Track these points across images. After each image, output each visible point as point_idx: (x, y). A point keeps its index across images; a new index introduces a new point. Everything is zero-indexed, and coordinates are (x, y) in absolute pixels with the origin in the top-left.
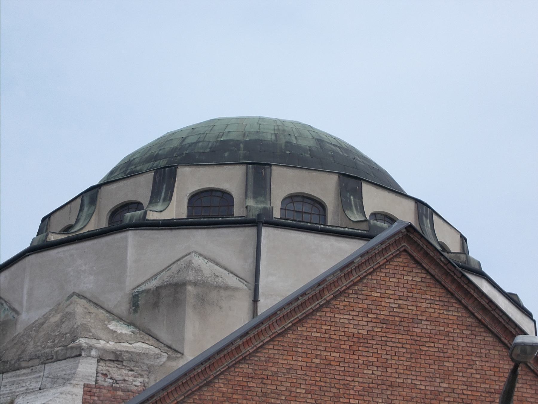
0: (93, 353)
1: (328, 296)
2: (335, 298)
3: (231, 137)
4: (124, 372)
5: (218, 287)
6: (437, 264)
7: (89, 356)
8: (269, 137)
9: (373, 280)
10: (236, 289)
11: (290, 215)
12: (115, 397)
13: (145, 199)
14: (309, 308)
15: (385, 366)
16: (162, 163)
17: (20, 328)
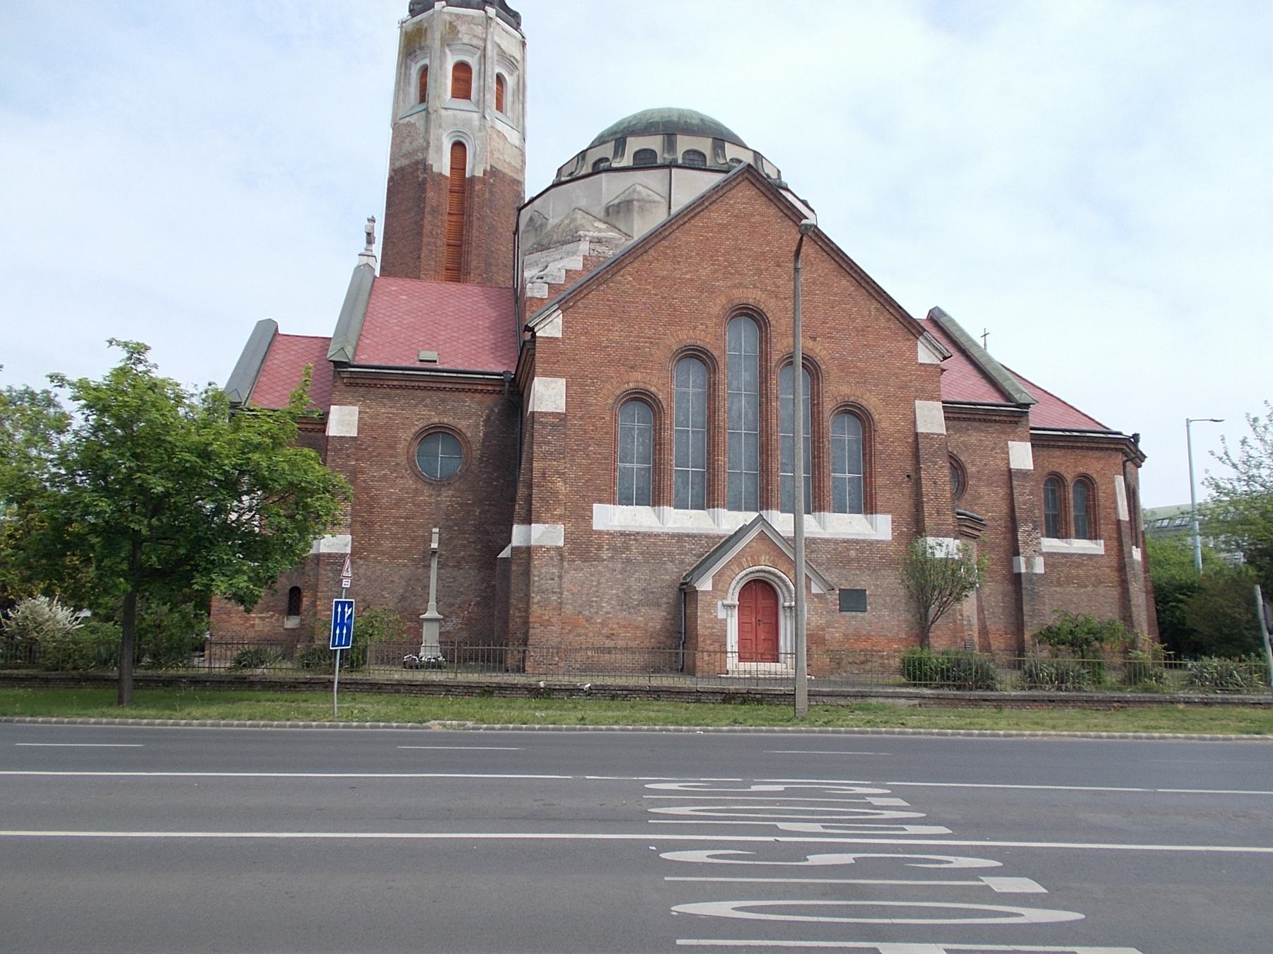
0: (587, 238)
1: (707, 204)
2: (710, 204)
4: (604, 248)
6: (764, 185)
7: (585, 240)
8: (675, 119)
10: (659, 202)
12: (599, 261)
13: (610, 155)
14: (697, 211)
16: (619, 136)
17: (549, 227)
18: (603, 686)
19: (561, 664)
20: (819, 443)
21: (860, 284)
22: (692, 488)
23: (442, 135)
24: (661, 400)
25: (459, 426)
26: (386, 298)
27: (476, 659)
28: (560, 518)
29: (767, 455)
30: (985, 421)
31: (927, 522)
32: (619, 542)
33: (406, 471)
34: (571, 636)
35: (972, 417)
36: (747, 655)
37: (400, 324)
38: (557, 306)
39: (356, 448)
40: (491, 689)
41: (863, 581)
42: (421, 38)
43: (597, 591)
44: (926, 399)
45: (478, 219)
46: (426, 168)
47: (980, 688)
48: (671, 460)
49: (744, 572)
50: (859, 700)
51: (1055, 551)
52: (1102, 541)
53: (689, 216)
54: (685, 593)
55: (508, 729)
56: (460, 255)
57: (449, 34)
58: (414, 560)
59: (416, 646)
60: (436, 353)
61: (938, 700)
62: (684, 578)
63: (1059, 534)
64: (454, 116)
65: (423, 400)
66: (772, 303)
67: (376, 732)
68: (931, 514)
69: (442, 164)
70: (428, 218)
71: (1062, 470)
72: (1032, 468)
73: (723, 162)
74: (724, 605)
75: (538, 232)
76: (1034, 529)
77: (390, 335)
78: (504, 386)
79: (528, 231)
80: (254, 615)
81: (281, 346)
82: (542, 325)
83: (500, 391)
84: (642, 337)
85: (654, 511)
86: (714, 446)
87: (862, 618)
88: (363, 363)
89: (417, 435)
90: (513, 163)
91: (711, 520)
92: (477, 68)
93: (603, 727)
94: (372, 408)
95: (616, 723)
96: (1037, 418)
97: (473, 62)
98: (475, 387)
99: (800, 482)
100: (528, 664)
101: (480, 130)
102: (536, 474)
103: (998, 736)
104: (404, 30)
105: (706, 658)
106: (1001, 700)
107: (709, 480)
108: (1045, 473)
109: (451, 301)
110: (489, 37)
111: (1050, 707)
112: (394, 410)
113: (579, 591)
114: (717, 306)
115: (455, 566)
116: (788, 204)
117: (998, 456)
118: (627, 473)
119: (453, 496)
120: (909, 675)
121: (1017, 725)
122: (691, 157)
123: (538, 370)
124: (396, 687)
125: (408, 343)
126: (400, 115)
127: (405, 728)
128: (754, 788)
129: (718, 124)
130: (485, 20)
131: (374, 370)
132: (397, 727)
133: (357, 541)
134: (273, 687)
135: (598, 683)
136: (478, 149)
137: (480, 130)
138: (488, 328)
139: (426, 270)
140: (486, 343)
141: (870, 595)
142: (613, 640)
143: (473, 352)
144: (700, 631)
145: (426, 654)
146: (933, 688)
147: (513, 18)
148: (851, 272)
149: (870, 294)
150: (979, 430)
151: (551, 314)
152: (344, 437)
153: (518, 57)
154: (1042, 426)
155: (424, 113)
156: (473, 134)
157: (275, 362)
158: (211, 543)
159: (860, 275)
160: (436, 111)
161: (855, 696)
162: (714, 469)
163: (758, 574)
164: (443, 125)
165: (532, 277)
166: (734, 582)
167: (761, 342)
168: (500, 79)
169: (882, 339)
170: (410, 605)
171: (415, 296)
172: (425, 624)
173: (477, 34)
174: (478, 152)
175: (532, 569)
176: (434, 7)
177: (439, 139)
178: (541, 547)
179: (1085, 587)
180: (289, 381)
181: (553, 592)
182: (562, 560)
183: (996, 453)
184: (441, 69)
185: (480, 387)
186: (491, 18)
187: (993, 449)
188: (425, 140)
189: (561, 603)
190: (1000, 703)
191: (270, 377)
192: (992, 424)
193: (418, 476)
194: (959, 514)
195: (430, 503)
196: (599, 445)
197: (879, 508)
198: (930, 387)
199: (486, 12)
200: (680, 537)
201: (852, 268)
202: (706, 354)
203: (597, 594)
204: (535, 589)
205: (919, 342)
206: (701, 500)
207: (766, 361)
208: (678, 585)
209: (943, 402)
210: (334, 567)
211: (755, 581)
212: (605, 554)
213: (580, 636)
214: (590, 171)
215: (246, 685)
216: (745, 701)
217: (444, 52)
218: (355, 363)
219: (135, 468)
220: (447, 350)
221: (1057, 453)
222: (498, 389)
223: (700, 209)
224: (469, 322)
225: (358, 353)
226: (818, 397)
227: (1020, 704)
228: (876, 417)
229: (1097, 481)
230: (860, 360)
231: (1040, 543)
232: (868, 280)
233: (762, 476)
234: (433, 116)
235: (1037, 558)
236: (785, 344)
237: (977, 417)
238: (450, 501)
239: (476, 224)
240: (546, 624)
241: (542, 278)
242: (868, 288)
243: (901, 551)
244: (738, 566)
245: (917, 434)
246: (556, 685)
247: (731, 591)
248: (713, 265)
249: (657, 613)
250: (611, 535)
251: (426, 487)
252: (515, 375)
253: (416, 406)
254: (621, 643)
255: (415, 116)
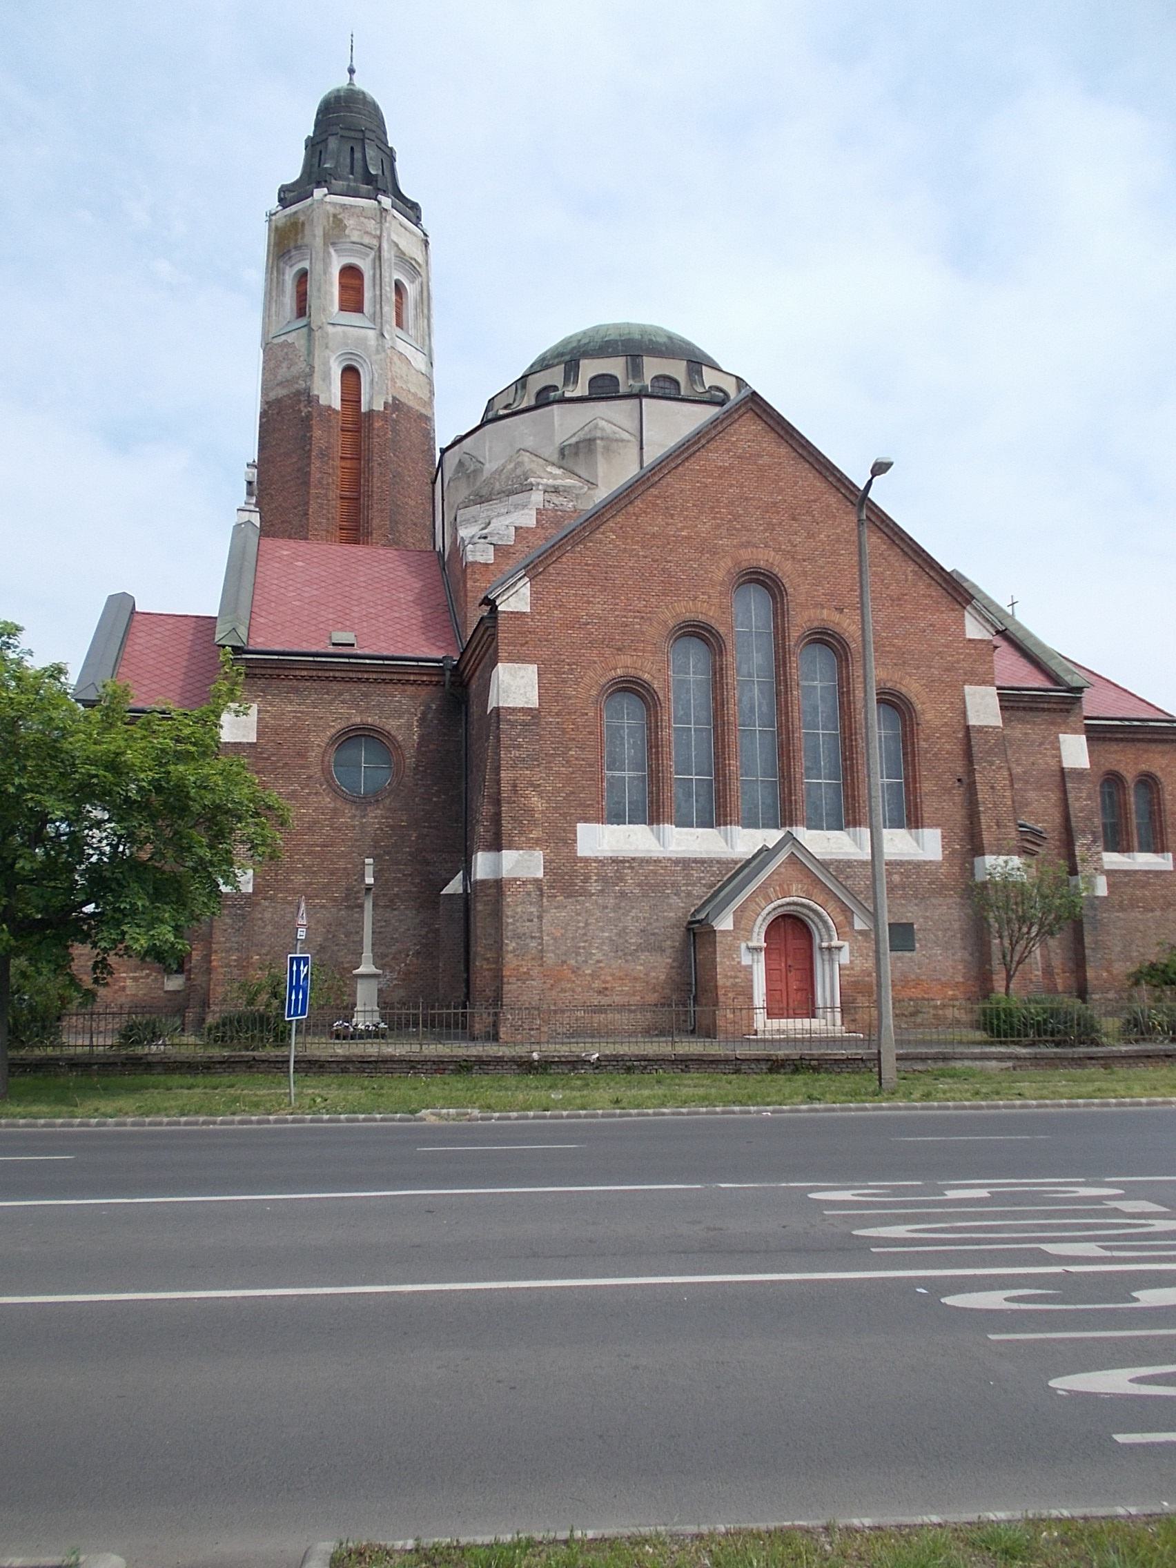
0: (540, 487)
1: (703, 441)
2: (708, 442)
3: (612, 337)
4: (561, 499)
5: (617, 440)
6: (772, 417)
7: (538, 489)
8: (637, 336)
9: (731, 430)
10: (628, 441)
11: (657, 390)
12: (556, 515)
13: (560, 384)
14: (691, 450)
15: (742, 486)
16: (567, 358)
17: (486, 475)
18: (615, 1055)
19: (545, 1029)
20: (852, 740)
21: (894, 542)
22: (697, 801)
23: (329, 358)
24: (657, 690)
25: (387, 728)
26: (277, 565)
27: (416, 1025)
28: (537, 843)
29: (789, 757)
30: (1031, 709)
31: (986, 836)
32: (610, 871)
33: (321, 785)
34: (554, 993)
35: (1016, 705)
36: (776, 1011)
37: (299, 597)
38: (523, 572)
39: (255, 757)
40: (470, 1064)
41: (911, 913)
42: (296, 234)
43: (585, 934)
44: (976, 684)
45: (379, 464)
46: (311, 400)
47: (1084, 1043)
48: (671, 766)
49: (772, 905)
50: (941, 1064)
51: (1116, 868)
52: (1170, 855)
53: (683, 457)
54: (694, 934)
55: (527, 1118)
56: (358, 511)
57: (333, 229)
58: (335, 900)
59: (348, 1011)
60: (352, 635)
61: (1035, 1059)
62: (693, 915)
63: (1119, 848)
64: (344, 332)
65: (341, 694)
66: (788, 566)
67: (339, 1127)
68: (990, 827)
69: (331, 394)
70: (316, 464)
71: (1121, 768)
72: (1088, 766)
73: (702, 390)
74: (748, 948)
75: (471, 480)
76: (1094, 841)
77: (289, 612)
78: (444, 675)
79: (459, 478)
80: (124, 975)
81: (142, 628)
82: (505, 597)
83: (438, 682)
84: (630, 611)
85: (849, 834)
86: (723, 747)
87: (910, 958)
88: (259, 648)
89: (334, 739)
90: (420, 395)
91: (723, 841)
92: (371, 273)
93: (651, 1111)
94: (274, 706)
95: (663, 1105)
96: (1092, 704)
97: (365, 265)
98: (406, 677)
99: (877, 790)
100: (502, 1030)
101: (378, 352)
102: (505, 786)
103: (1140, 1104)
104: (273, 224)
105: (730, 1016)
106: (1109, 1057)
107: (718, 791)
108: (1101, 773)
109: (361, 568)
110: (385, 234)
111: (1167, 1064)
112: (303, 708)
113: (562, 935)
114: (721, 571)
115: (387, 906)
116: (803, 442)
117: (1049, 753)
118: (616, 784)
119: (383, 817)
120: (992, 1031)
121: (1155, 1089)
122: (661, 384)
123: (502, 654)
124: (343, 1065)
125: (314, 622)
126: (273, 333)
127: (393, 1120)
128: (952, 1194)
129: (689, 344)
130: (378, 213)
131: (276, 657)
132: (382, 1120)
133: (260, 877)
134: (177, 1068)
135: (608, 1052)
136: (376, 375)
137: (378, 352)
138: (413, 602)
139: (316, 529)
140: (414, 621)
141: (919, 930)
142: (606, 996)
143: (399, 632)
144: (721, 981)
145: (361, 1021)
146: (1026, 1046)
147: (412, 210)
148: (882, 527)
149: (905, 553)
150: (1024, 721)
151: (516, 582)
152: (240, 743)
153: (420, 259)
154: (1095, 715)
155: (305, 330)
156: (369, 357)
157: (136, 647)
158: (119, 884)
159: (892, 529)
160: (320, 328)
161: (935, 1058)
162: (724, 776)
163: (788, 908)
164: (330, 345)
165: (473, 537)
166: (760, 918)
167: (775, 615)
168: (399, 288)
169: (922, 610)
170: (330, 957)
171: (313, 562)
172: (359, 981)
173: (369, 230)
174: (376, 380)
175: (505, 909)
176: (312, 195)
177: (326, 363)
178: (516, 880)
179: (1152, 910)
180: (158, 672)
181: (532, 937)
182: (542, 895)
183: (1046, 749)
184: (325, 273)
185: (412, 678)
186: (386, 210)
187: (1041, 744)
188: (308, 365)
189: (541, 951)
190: (1108, 1061)
191: (132, 667)
192: (1039, 714)
193: (335, 791)
194: (1021, 826)
195: (354, 826)
196: (582, 749)
197: (926, 821)
198: (981, 669)
199: (379, 202)
200: (686, 864)
201: (883, 521)
202: (710, 632)
203: (585, 938)
204: (509, 934)
205: (966, 614)
206: (707, 815)
207: (784, 639)
208: (685, 924)
209: (999, 688)
210: (233, 910)
211: (784, 917)
212: (594, 887)
213: (565, 992)
214: (533, 402)
215: (143, 1067)
216: (797, 1069)
217: (329, 253)
218: (250, 648)
219: (26, 786)
220: (365, 630)
221: (1114, 747)
222: (435, 679)
223: (695, 448)
224: (387, 594)
225: (251, 635)
226: (849, 684)
227: (1131, 1061)
228: (919, 707)
229: (1162, 780)
230: (897, 637)
231: (1101, 859)
232: (903, 535)
233: (782, 784)
234: (317, 334)
235: (1099, 877)
236: (806, 618)
237: (1021, 705)
238: (379, 823)
239: (377, 471)
240: (525, 977)
241: (485, 538)
242: (902, 546)
243: (954, 874)
244: (764, 899)
245: (968, 727)
246: (554, 1057)
247: (756, 929)
248: (714, 518)
249: (660, 959)
250: (600, 862)
251: (348, 806)
252: (459, 661)
253: (331, 703)
254: (617, 999)
255: (294, 334)
